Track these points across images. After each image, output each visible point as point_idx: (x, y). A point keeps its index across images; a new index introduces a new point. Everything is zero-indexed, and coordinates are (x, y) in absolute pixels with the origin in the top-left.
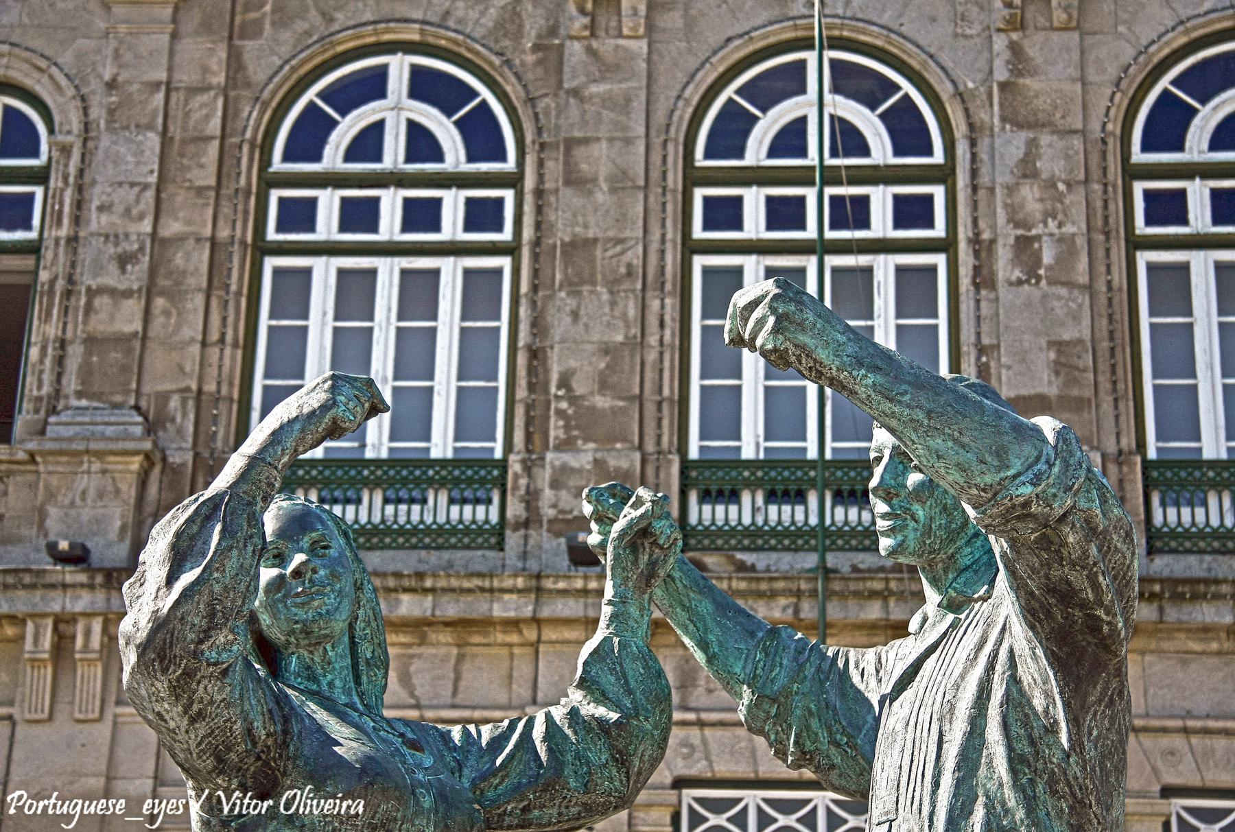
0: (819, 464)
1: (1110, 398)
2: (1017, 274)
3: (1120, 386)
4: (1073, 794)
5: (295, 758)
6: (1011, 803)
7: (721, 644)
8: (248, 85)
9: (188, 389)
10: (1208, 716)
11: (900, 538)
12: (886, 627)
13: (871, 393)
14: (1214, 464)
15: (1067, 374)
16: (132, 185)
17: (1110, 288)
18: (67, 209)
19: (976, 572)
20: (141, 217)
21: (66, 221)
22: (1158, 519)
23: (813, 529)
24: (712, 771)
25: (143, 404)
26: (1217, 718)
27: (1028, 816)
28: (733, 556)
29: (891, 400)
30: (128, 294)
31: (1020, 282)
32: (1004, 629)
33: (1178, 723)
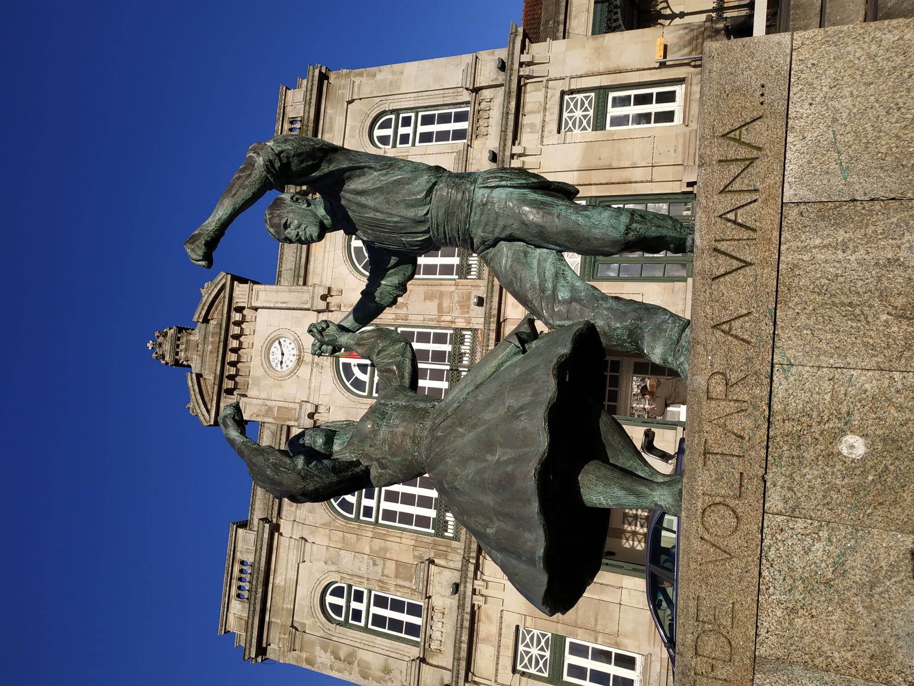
2: (405, 309)
8: (330, 523)
9: (413, 549)
16: (354, 560)
18: (359, 580)
20: (363, 558)
21: (362, 580)
22: (474, 277)
25: (416, 563)
30: (384, 564)
31: (407, 308)
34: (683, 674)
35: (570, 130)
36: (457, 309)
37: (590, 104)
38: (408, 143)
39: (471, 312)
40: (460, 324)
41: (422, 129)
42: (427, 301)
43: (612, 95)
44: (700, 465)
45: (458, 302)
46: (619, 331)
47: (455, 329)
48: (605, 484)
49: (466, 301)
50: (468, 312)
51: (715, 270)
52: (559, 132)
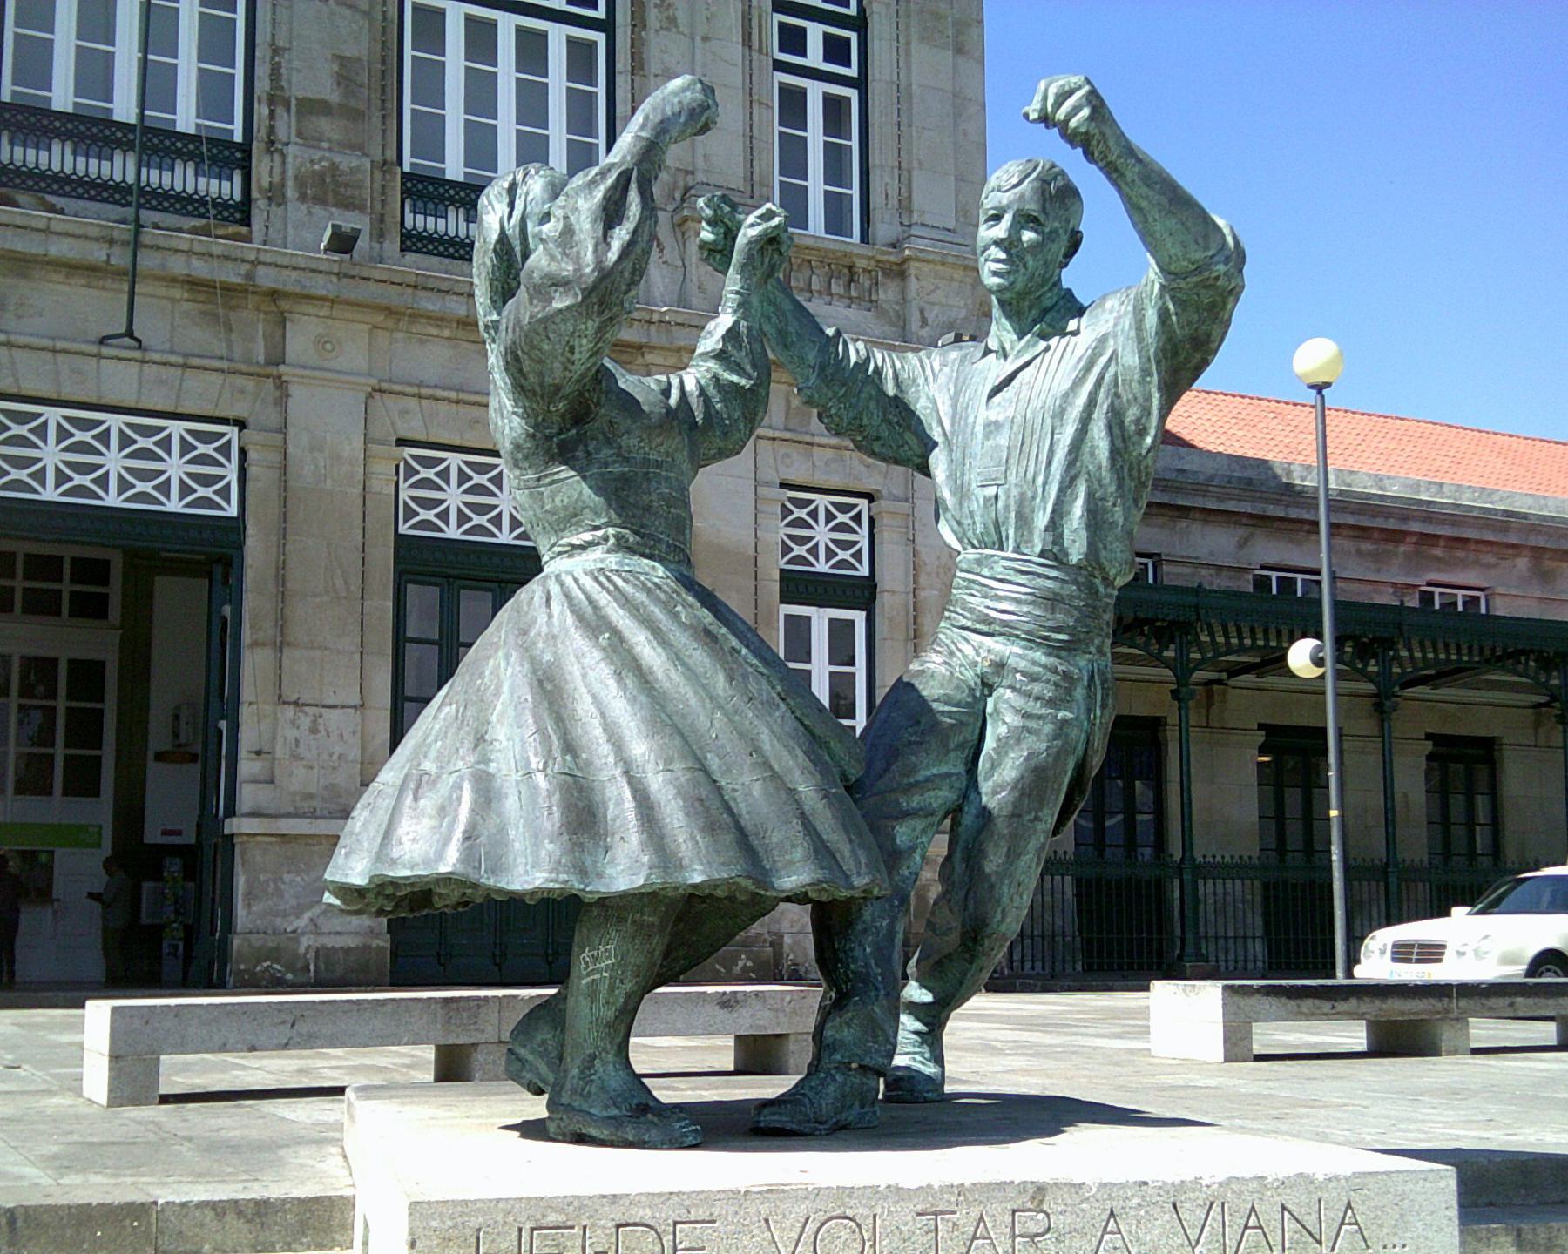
0: (138, 128)
1: (379, 114)
3: (388, 105)
4: (1139, 478)
5: (607, 393)
6: (1106, 481)
7: (798, 335)
10: (436, 386)
11: (1012, 278)
12: (183, 282)
13: (1136, 178)
14: (453, 184)
15: (347, 86)
17: (384, 19)
19: (1058, 311)
22: (409, 223)
23: (130, 186)
24: (19, 387)
26: (443, 389)
27: (1117, 490)
28: (43, 198)
29: (1148, 186)
32: (1110, 359)
33: (416, 390)
34: (580, 1208)
35: (786, 512)
36: (312, 162)
37: (843, 564)
38: (781, 50)
39: (304, 207)
40: (263, 169)
41: (815, 92)
42: (336, 67)
43: (859, 617)
44: (919, 1208)
45: (334, 167)
46: (857, 953)
47: (246, 148)
48: (639, 967)
49: (336, 193)
50: (303, 197)
51: (1187, 1205)
52: (783, 485)
